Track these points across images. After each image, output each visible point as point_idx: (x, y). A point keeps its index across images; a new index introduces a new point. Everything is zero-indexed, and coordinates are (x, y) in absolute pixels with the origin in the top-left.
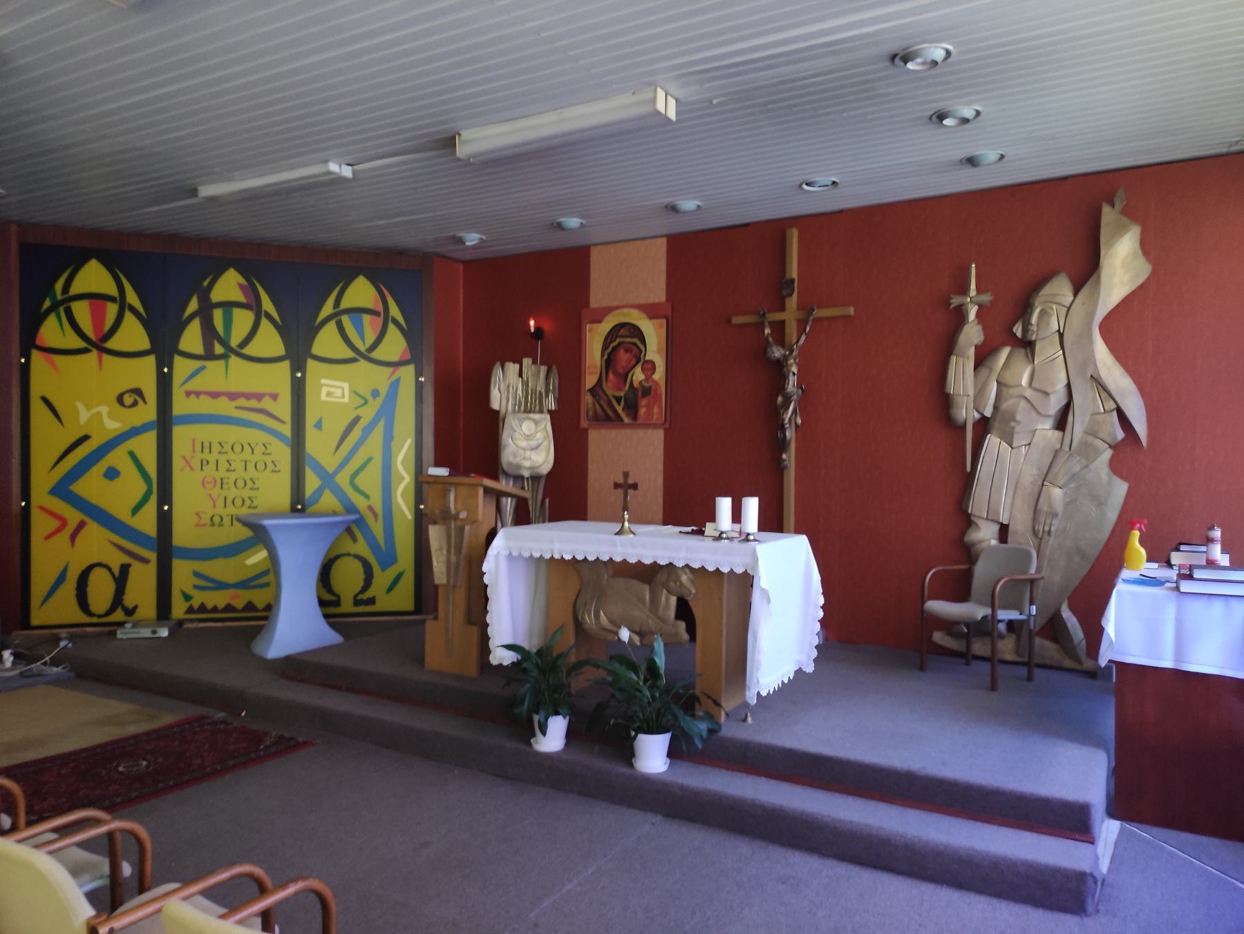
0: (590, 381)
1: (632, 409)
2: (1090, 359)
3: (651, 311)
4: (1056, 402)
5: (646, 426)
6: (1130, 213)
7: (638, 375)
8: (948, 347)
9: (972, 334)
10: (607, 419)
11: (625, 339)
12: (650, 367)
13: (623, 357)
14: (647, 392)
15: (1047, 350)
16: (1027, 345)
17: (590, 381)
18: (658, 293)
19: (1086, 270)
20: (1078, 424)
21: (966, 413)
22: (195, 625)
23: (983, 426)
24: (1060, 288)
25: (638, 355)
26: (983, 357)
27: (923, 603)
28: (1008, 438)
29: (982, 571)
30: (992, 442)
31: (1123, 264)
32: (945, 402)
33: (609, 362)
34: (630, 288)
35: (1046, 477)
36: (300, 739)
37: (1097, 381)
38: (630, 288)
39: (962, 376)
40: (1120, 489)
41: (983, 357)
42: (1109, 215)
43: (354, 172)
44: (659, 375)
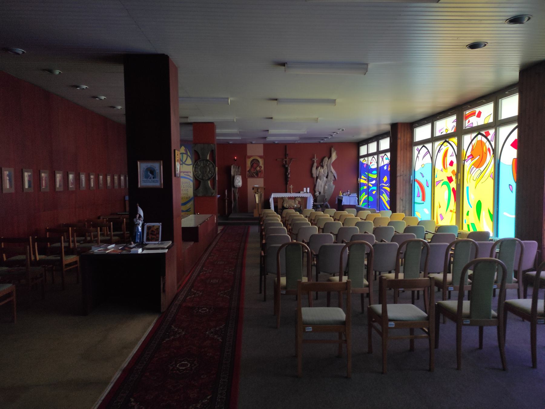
0: (248, 169)
1: (257, 174)
2: (330, 169)
3: (261, 157)
4: (326, 175)
5: (260, 177)
6: (335, 149)
7: (258, 169)
8: (312, 166)
9: (315, 164)
10: (252, 176)
11: (255, 162)
12: (261, 167)
13: (255, 165)
14: (260, 172)
15: (325, 167)
16: (322, 166)
17: (248, 169)
18: (262, 154)
19: (330, 157)
20: (329, 177)
21: (315, 176)
22: (28, 248)
23: (317, 178)
24: (326, 159)
25: (258, 165)
26: (317, 168)
27: (474, 272)
28: (320, 180)
29: (318, 198)
30: (318, 180)
31: (334, 156)
32: (312, 174)
33: (252, 166)
34: (255, 151)
35: (325, 185)
36: (408, 140)
37: (331, 172)
38: (255, 151)
39: (314, 169)
40: (334, 187)
41: (317, 168)
42: (333, 149)
43: (471, 321)
44: (262, 169)
